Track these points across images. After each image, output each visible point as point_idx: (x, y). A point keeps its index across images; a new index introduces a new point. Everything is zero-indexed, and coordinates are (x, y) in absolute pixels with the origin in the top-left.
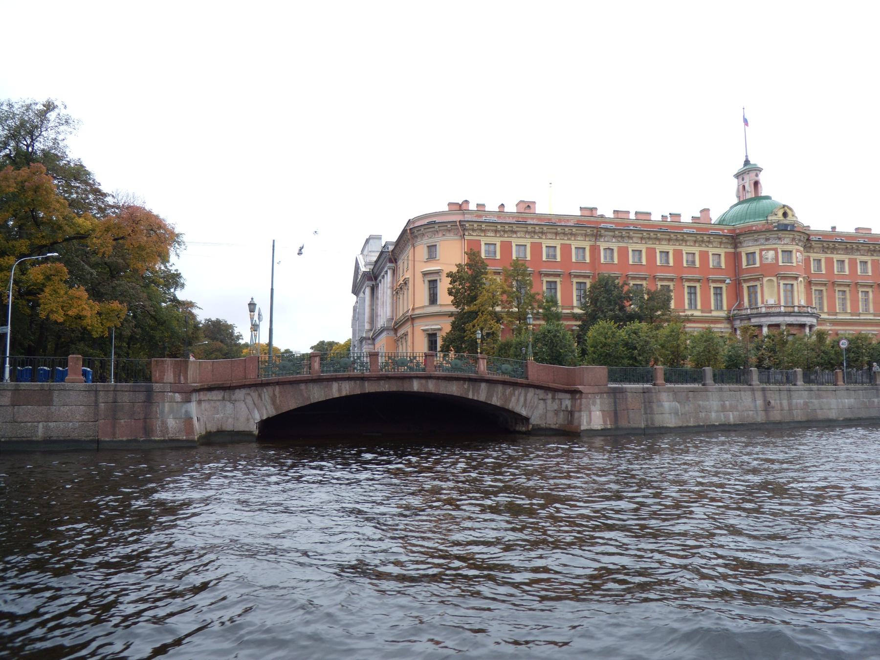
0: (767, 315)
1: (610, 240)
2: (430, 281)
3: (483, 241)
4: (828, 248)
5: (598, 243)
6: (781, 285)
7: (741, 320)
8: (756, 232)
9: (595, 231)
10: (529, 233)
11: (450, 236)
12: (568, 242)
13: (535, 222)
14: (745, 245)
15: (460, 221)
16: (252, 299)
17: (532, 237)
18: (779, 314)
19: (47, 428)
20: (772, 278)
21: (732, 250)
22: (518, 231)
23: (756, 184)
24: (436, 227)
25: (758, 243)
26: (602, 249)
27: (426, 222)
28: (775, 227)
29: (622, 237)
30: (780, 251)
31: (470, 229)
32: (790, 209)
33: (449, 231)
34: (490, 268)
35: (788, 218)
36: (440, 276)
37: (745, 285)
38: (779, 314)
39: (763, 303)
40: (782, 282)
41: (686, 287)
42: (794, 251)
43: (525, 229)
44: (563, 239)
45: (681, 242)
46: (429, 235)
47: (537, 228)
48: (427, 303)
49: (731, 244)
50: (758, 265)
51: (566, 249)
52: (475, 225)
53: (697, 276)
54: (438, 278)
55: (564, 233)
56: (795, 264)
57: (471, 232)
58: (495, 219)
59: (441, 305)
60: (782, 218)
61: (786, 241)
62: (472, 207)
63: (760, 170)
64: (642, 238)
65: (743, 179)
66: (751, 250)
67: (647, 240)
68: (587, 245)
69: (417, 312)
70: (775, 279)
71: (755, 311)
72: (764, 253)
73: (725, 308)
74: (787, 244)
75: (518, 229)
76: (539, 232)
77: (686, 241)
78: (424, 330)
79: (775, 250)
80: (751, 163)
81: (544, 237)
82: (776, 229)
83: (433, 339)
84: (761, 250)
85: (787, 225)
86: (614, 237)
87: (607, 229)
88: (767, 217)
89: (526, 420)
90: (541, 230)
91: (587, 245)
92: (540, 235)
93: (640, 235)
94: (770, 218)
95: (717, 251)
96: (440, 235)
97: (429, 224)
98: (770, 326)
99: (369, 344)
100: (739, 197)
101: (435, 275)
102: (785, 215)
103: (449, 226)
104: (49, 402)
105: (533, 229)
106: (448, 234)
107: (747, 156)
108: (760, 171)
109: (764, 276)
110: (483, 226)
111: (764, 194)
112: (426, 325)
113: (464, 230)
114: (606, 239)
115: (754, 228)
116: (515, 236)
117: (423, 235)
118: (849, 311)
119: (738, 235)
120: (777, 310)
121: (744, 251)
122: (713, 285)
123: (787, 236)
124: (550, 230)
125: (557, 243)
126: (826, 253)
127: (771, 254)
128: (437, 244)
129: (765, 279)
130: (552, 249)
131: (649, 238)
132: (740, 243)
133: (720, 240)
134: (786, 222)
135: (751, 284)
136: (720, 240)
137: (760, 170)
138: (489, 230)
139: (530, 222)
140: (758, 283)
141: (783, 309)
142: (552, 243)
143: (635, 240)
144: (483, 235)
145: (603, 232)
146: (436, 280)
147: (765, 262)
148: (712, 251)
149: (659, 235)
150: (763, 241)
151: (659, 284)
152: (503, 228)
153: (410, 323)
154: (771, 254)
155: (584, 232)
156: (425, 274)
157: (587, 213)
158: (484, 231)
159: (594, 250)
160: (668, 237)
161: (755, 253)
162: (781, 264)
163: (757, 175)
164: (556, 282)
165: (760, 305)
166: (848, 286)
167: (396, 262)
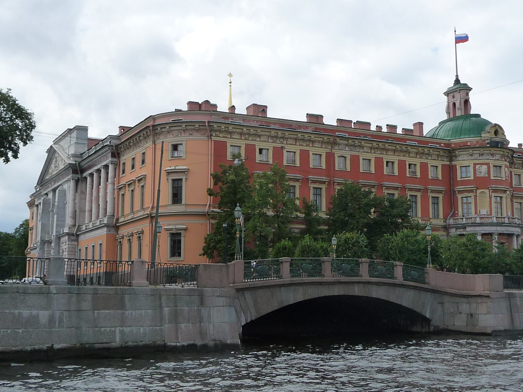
0: (481, 225)
2: (173, 180)
3: (230, 142)
5: (454, 163)
6: (493, 200)
7: (457, 228)
8: (470, 148)
9: (332, 139)
10: (273, 137)
11: (197, 136)
12: (307, 148)
14: (460, 158)
15: (209, 122)
17: (274, 142)
18: (492, 224)
19: (122, 333)
20: (484, 190)
21: (448, 163)
23: (467, 102)
24: (184, 126)
25: (472, 158)
26: (336, 156)
28: (487, 144)
30: (491, 166)
33: (197, 130)
34: (289, 175)
37: (459, 196)
38: (492, 224)
40: (493, 195)
41: (312, 188)
42: (504, 166)
43: (268, 133)
44: (303, 145)
46: (175, 133)
47: (280, 133)
48: (170, 202)
49: (447, 157)
52: (223, 127)
53: (418, 186)
55: (360, 146)
56: (504, 179)
57: (218, 133)
59: (186, 205)
60: (494, 136)
61: (498, 157)
62: (373, 128)
63: (470, 89)
64: (241, 134)
65: (454, 97)
66: (466, 163)
67: (376, 150)
68: (323, 151)
71: (470, 221)
72: (477, 167)
73: (441, 216)
75: (262, 133)
76: (281, 138)
77: (409, 153)
79: (488, 164)
80: (462, 82)
82: (488, 145)
83: (177, 238)
84: (475, 165)
85: (498, 143)
87: (342, 138)
89: (427, 321)
90: (283, 135)
91: (323, 151)
93: (370, 145)
95: (435, 163)
97: (174, 122)
98: (483, 235)
99: (72, 240)
100: (448, 113)
101: (180, 174)
102: (496, 133)
103: (197, 126)
104: (122, 306)
105: (276, 134)
106: (195, 133)
107: (457, 76)
108: (470, 90)
109: (477, 188)
110: (230, 128)
112: (169, 225)
114: (340, 147)
115: (469, 144)
119: (454, 150)
120: (489, 221)
121: (458, 163)
122: (312, 186)
123: (498, 152)
124: (291, 136)
128: (184, 143)
129: (479, 191)
132: (456, 156)
133: (438, 153)
134: (497, 139)
135: (466, 194)
136: (438, 153)
137: (470, 89)
138: (235, 133)
139: (272, 127)
141: (495, 220)
143: (365, 149)
145: (338, 140)
146: (181, 180)
148: (431, 163)
149: (386, 146)
150: (476, 156)
151: (386, 192)
152: (248, 131)
153: (148, 220)
155: (321, 139)
156: (169, 173)
157: (314, 120)
158: (231, 133)
159: (330, 157)
160: (394, 148)
162: (492, 178)
164: (295, 186)
167: (119, 157)
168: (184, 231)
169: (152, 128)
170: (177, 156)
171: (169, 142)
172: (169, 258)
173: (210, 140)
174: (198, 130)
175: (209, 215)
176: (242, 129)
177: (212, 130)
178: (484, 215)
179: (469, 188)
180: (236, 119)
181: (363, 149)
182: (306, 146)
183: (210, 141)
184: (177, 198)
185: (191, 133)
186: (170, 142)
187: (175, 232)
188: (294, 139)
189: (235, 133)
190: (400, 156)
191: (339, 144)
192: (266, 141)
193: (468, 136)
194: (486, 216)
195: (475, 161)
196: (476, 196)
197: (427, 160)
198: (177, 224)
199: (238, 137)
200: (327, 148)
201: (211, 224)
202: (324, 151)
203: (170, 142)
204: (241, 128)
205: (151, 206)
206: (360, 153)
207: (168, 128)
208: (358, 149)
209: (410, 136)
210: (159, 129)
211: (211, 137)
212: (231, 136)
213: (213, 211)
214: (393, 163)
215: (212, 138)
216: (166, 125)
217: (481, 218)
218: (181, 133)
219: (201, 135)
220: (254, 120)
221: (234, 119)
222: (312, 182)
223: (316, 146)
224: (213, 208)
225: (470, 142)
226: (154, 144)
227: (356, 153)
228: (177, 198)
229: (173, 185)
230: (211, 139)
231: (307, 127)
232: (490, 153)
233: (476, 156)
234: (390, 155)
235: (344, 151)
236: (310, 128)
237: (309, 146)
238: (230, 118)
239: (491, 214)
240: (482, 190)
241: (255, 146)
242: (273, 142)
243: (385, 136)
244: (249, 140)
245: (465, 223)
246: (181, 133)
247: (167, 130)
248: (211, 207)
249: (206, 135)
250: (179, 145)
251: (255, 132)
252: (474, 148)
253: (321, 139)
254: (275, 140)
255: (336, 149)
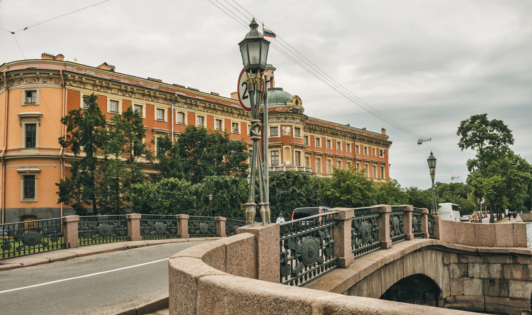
1: (183, 106)
4: (312, 129)
6: (294, 152)
8: (278, 112)
11: (51, 84)
12: (152, 103)
13: (127, 82)
15: (63, 71)
16: (432, 154)
17: (124, 95)
20: (288, 146)
22: (113, 88)
24: (38, 73)
25: (280, 120)
27: (25, 67)
29: (191, 104)
30: (293, 127)
31: (71, 80)
32: (300, 99)
35: (298, 105)
36: (40, 120)
39: (282, 163)
40: (295, 150)
43: (118, 87)
44: (148, 100)
45: (230, 114)
48: (23, 146)
50: (279, 136)
51: (150, 109)
54: (37, 123)
56: (301, 138)
57: (72, 83)
58: (93, 74)
59: (40, 149)
60: (295, 105)
61: (298, 121)
63: (274, 69)
64: (204, 107)
66: (274, 125)
69: (10, 154)
70: (290, 147)
72: (283, 128)
74: (298, 123)
76: (130, 92)
78: (19, 172)
81: (133, 96)
84: (282, 126)
85: (298, 110)
86: (185, 103)
88: (286, 103)
92: (130, 94)
93: (204, 105)
94: (288, 103)
96: (41, 81)
101: (34, 120)
102: (297, 102)
103: (51, 74)
105: (125, 88)
108: (274, 70)
109: (283, 144)
110: (84, 79)
111: (276, 86)
112: (23, 167)
113: (66, 79)
114: (180, 105)
115: (277, 110)
116: (110, 92)
117: (22, 79)
118: (322, 172)
123: (298, 117)
125: (143, 102)
126: (311, 132)
127: (288, 129)
128: (38, 89)
129: (284, 147)
130: (139, 107)
131: (210, 108)
134: (298, 108)
137: (274, 69)
138: (88, 83)
140: (279, 149)
142: (139, 102)
144: (82, 87)
145: (178, 98)
146: (35, 125)
147: (284, 134)
152: (100, 84)
154: (288, 129)
155: (164, 96)
156: (22, 118)
160: (222, 109)
161: (277, 127)
162: (294, 137)
163: (273, 73)
165: (280, 165)
166: (322, 155)
168: (38, 174)
169: (6, 75)
170: (30, 102)
171: (23, 89)
172: (22, 200)
173: (64, 88)
174: (50, 78)
175: (63, 159)
176: (95, 81)
177: (66, 79)
178: (288, 165)
179: (278, 144)
180: (90, 71)
181: (198, 108)
182: (229, 116)
183: (64, 90)
184: (30, 141)
185: (45, 80)
186: (24, 88)
187: (28, 175)
188: (141, 94)
189: (88, 83)
190: (226, 116)
191: (233, 114)
192: (116, 94)
193: (276, 104)
194: (289, 166)
195: (281, 123)
196: (282, 151)
197: (246, 121)
198: (30, 167)
199: (90, 87)
200: (168, 104)
201: (64, 167)
202: (167, 107)
203: (24, 88)
204: (94, 80)
205: (4, 150)
206: (196, 111)
207: (21, 74)
208: (194, 107)
209: (234, 100)
210: (13, 76)
211: (65, 86)
212: (84, 87)
213: (66, 155)
214: (237, 124)
215: (66, 86)
216: (19, 71)
217: (287, 168)
218: (35, 81)
219: (55, 83)
220: (105, 74)
221: (87, 71)
222: (156, 133)
223: (160, 102)
224: (66, 153)
225: (278, 108)
226: (7, 91)
227: (192, 110)
228: (30, 141)
229: (26, 130)
230: (65, 87)
231: (152, 84)
232: (293, 118)
233: (283, 120)
234: (161, 103)
235: (183, 108)
236: (155, 86)
237: (154, 102)
238: (83, 69)
239: (293, 164)
240: (287, 146)
241: (107, 98)
242: (122, 95)
243: (215, 99)
244: (101, 91)
245: (275, 171)
246: (35, 81)
247: (20, 77)
248: (65, 152)
249: (60, 83)
250: (33, 92)
251: (107, 85)
252: (281, 113)
253: (164, 96)
254: (124, 93)
255: (176, 106)
